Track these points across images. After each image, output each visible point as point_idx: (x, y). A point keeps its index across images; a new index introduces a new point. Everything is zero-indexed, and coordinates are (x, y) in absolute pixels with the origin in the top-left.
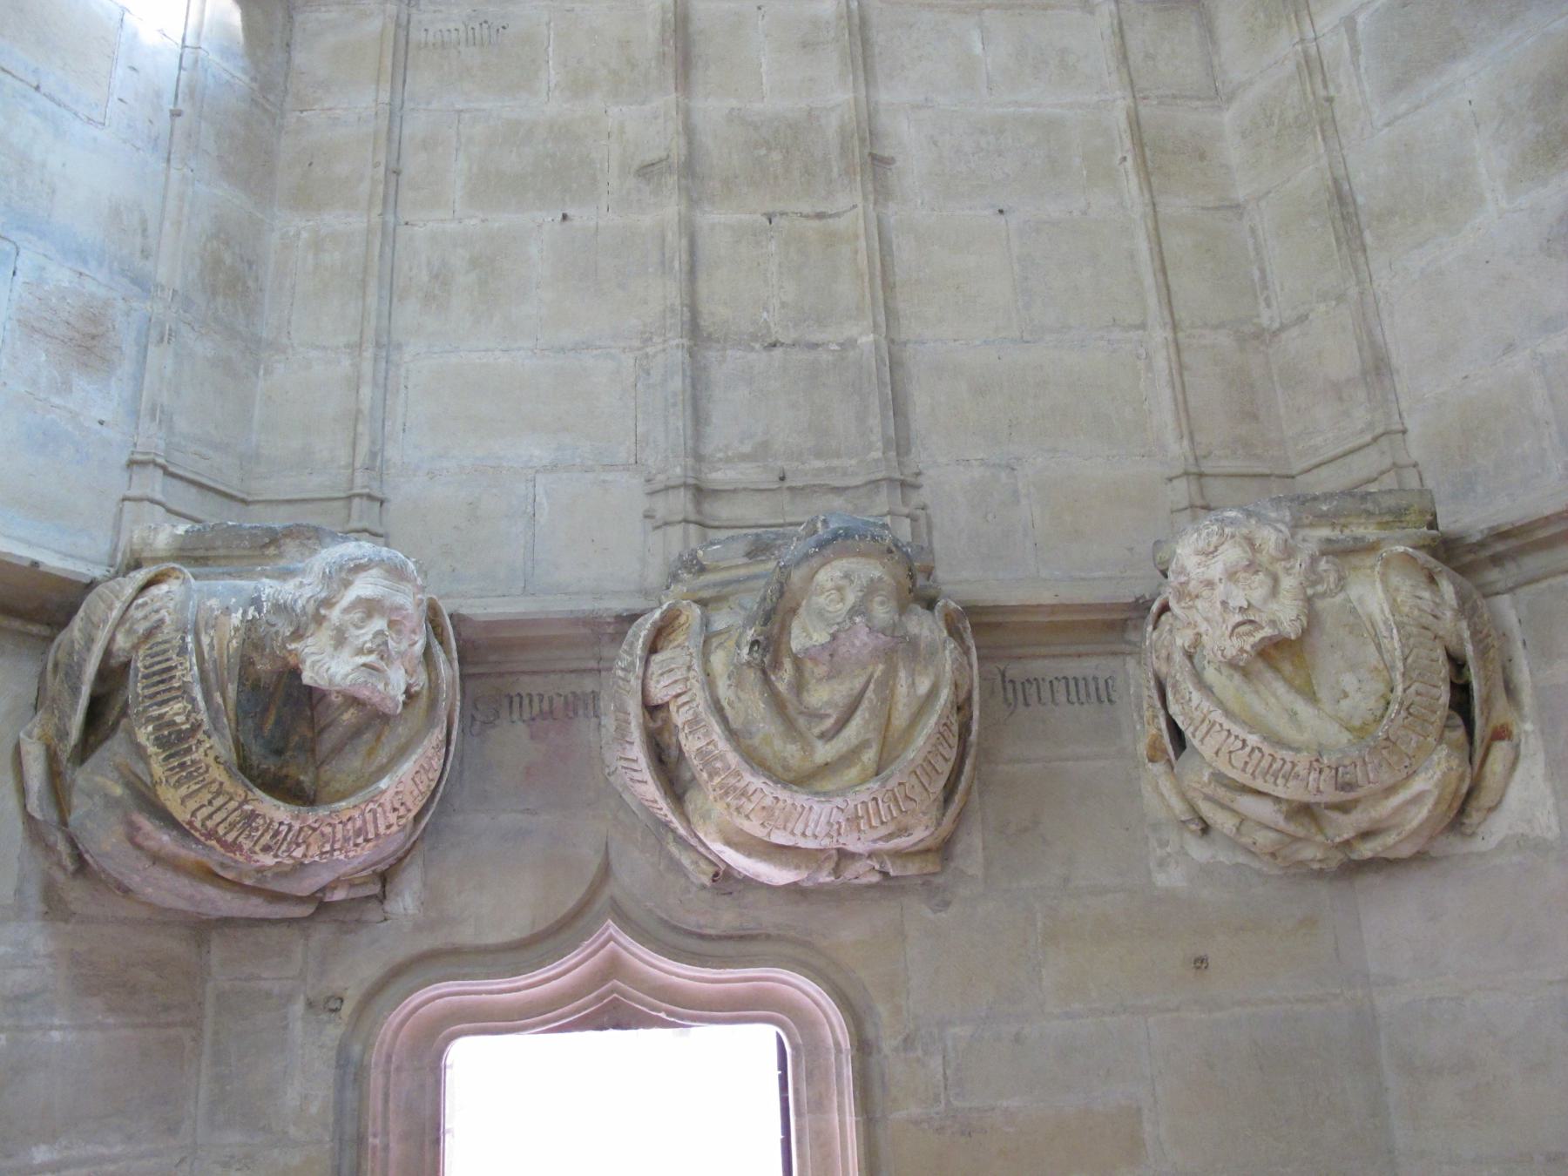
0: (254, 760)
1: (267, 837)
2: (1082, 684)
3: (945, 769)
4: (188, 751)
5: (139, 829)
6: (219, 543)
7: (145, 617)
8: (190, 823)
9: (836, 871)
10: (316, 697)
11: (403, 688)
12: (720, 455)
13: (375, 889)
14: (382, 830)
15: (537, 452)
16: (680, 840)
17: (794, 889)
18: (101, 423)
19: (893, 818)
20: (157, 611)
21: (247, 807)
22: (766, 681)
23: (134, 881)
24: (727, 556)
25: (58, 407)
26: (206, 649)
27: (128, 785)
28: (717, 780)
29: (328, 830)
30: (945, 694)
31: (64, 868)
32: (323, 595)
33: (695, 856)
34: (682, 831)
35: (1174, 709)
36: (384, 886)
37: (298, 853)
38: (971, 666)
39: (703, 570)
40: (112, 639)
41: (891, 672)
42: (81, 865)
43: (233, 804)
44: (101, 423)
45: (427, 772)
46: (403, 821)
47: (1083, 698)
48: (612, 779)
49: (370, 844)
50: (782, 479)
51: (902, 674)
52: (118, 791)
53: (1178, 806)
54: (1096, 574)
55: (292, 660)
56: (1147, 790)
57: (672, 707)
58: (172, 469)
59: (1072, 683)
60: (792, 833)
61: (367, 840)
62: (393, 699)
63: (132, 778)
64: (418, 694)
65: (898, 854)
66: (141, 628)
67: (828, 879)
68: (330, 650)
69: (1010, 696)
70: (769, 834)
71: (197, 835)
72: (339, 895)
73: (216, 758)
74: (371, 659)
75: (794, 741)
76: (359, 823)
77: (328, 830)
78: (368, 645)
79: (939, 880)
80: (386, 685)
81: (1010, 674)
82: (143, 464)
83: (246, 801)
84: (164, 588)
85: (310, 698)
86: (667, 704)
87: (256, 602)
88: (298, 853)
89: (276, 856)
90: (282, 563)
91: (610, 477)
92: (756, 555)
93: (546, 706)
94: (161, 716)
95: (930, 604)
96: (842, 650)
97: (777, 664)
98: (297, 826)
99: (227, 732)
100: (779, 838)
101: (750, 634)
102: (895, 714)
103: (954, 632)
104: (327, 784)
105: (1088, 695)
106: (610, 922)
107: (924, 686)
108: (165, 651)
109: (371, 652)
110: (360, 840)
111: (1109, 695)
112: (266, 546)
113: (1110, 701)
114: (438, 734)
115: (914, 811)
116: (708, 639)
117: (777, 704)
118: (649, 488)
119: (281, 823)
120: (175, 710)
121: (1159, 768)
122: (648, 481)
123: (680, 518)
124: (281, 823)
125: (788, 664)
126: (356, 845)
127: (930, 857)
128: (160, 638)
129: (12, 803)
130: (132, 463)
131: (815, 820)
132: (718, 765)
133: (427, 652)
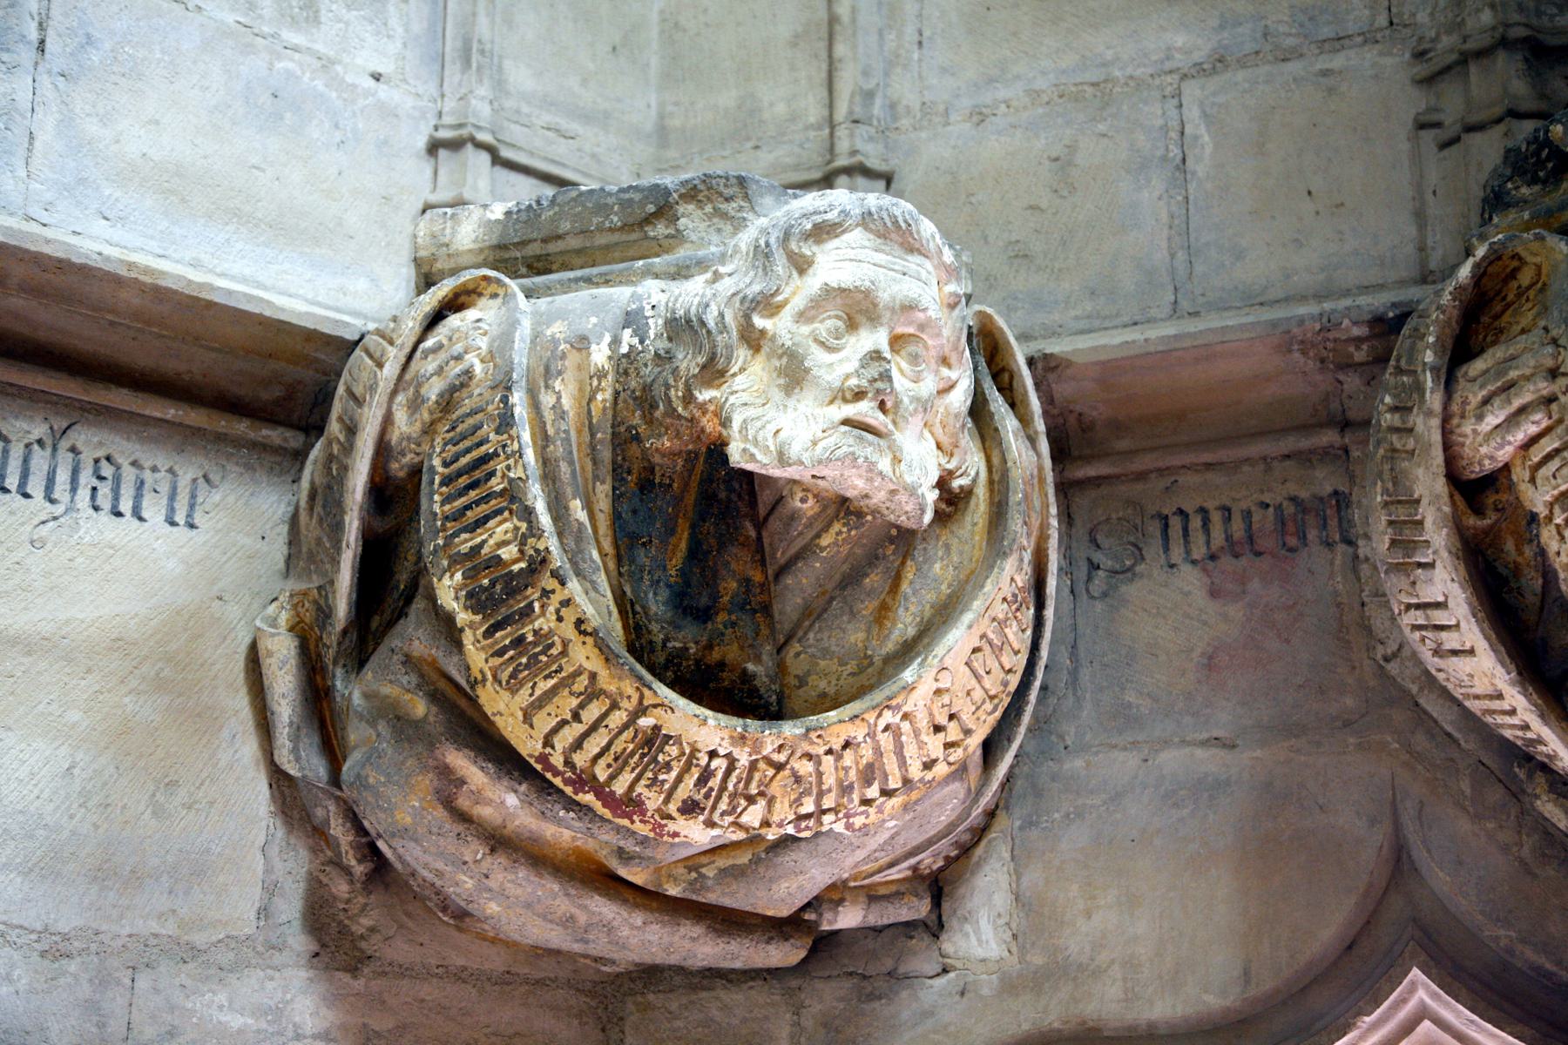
0: (657, 632)
1: (690, 781)
4: (527, 612)
5: (462, 782)
6: (566, 226)
7: (440, 371)
8: (543, 759)
10: (765, 498)
11: (934, 476)
13: (919, 908)
14: (915, 771)
15: (1180, 40)
18: (377, 77)
20: (458, 358)
21: (645, 722)
23: (462, 886)
25: (296, 49)
26: (549, 416)
27: (435, 697)
29: (805, 768)
31: (347, 871)
32: (756, 288)
36: (937, 901)
37: (753, 816)
40: (388, 420)
42: (380, 870)
43: (618, 718)
44: (377, 77)
45: (997, 651)
46: (957, 755)
48: (1393, 668)
49: (896, 801)
52: (420, 707)
55: (709, 425)
57: (1520, 474)
58: (506, 153)
61: (887, 793)
62: (912, 491)
63: (442, 684)
64: (967, 493)
66: (433, 390)
68: (777, 395)
71: (558, 781)
72: (849, 918)
73: (579, 622)
74: (864, 409)
76: (867, 753)
77: (805, 768)
78: (853, 382)
80: (897, 460)
82: (455, 145)
83: (641, 710)
84: (471, 314)
85: (753, 503)
86: (1507, 467)
87: (632, 319)
88: (753, 816)
89: (710, 824)
90: (682, 253)
91: (1338, 62)
93: (1238, 528)
94: (476, 550)
98: (744, 759)
99: (602, 579)
104: (802, 682)
106: (1416, 973)
108: (479, 427)
109: (859, 395)
110: (873, 792)
112: (648, 220)
114: (1012, 574)
118: (1422, 70)
119: (713, 754)
120: (500, 537)
122: (1420, 55)
123: (1498, 111)
124: (713, 754)
126: (867, 802)
128: (468, 405)
129: (249, 748)
130: (434, 147)
133: (978, 411)
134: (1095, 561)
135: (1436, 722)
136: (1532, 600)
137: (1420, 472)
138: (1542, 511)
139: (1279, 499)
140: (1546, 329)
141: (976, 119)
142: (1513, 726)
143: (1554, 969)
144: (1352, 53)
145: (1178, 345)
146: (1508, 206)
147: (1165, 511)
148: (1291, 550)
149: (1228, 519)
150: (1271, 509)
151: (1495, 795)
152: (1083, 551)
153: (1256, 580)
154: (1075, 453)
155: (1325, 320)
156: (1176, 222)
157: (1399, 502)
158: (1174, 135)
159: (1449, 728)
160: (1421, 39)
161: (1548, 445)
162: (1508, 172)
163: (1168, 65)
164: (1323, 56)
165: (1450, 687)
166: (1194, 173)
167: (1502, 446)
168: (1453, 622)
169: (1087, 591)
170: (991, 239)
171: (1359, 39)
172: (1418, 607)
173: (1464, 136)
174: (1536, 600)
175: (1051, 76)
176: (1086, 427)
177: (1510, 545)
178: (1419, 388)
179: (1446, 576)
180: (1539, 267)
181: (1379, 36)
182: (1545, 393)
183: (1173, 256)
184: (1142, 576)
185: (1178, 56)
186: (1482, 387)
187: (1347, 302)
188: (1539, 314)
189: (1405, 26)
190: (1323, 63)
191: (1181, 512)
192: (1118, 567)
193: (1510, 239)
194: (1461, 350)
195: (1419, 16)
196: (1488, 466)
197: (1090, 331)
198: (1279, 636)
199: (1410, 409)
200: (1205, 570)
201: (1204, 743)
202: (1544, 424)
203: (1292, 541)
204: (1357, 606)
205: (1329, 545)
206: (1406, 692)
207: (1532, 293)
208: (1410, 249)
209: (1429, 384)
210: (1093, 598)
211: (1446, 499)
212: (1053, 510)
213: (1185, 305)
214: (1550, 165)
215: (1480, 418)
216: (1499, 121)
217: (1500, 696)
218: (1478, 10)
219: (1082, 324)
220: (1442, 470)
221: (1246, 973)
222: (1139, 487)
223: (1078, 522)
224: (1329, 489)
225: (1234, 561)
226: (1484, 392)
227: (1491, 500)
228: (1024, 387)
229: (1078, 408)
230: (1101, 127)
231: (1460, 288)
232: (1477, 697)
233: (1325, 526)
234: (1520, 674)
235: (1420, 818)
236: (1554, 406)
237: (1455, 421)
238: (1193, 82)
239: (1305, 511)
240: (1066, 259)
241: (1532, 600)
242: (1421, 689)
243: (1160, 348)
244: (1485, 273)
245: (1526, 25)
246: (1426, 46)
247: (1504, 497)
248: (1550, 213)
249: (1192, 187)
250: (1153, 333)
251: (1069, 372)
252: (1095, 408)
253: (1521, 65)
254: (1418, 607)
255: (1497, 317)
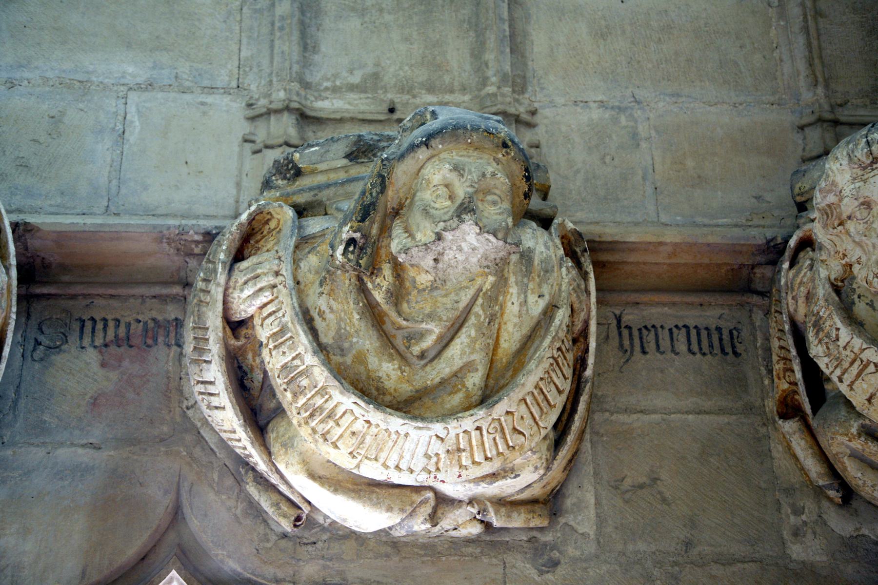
2: (704, 334)
3: (559, 402)
9: (433, 518)
12: (326, 84)
15: (130, 69)
16: (262, 481)
17: (384, 539)
19: (499, 454)
22: (362, 290)
24: (325, 160)
28: (302, 401)
30: (561, 316)
33: (275, 497)
34: (262, 467)
35: (816, 350)
38: (588, 293)
39: (298, 173)
41: (502, 282)
47: (706, 349)
48: (190, 413)
50: (392, 110)
51: (514, 290)
53: (813, 467)
54: (721, 221)
56: (777, 450)
57: (257, 321)
59: (693, 332)
60: (386, 466)
65: (503, 503)
67: (423, 527)
69: (626, 343)
70: (358, 466)
75: (391, 359)
79: (548, 537)
81: (627, 319)
86: (252, 317)
91: (210, 99)
92: (356, 158)
93: (122, 332)
95: (545, 222)
96: (449, 255)
97: (374, 270)
100: (371, 471)
101: (346, 233)
102: (504, 336)
103: (571, 253)
105: (711, 346)
106: (174, 573)
107: (537, 306)
111: (733, 347)
113: (736, 354)
115: (522, 447)
116: (304, 243)
117: (374, 316)
118: (250, 113)
121: (790, 426)
122: (250, 105)
123: (281, 141)
125: (387, 270)
127: (537, 507)
131: (408, 449)
132: (305, 382)
134: (39, 340)
135: (207, 442)
136: (257, 384)
137: (210, 314)
138: (265, 341)
139: (147, 319)
140: (277, 251)
141: (8, 85)
142: (240, 447)
143: (241, 571)
144: (217, 96)
145: (102, 229)
146: (271, 188)
147: (84, 318)
148: (148, 346)
149: (117, 326)
150: (141, 324)
151: (229, 481)
152: (33, 334)
153: (128, 360)
154: (37, 279)
155: (181, 229)
156: (115, 164)
157: (200, 328)
158: (120, 118)
159: (213, 446)
160: (251, 97)
161: (270, 308)
162: (274, 171)
163: (123, 81)
164: (203, 95)
165: (214, 425)
166: (128, 140)
167: (250, 306)
168: (217, 392)
169: (32, 356)
170: (7, 153)
171: (222, 91)
172: (203, 383)
173: (264, 150)
174: (259, 385)
175: (57, 72)
176: (46, 266)
177: (250, 356)
178: (215, 271)
179: (216, 369)
180: (279, 220)
181: (232, 91)
182: (272, 282)
183: (110, 182)
184: (65, 351)
185: (128, 77)
186: (245, 275)
187: (194, 222)
188: (276, 244)
189: (245, 90)
190: (203, 98)
191: (93, 319)
192: (52, 345)
193: (268, 204)
194: (239, 256)
195: (252, 86)
196: (244, 316)
197: (57, 214)
198: (134, 391)
199: (210, 281)
200: (100, 352)
201: (83, 446)
202: (270, 298)
203: (150, 342)
204: (177, 379)
205: (169, 346)
206: (194, 426)
207: (274, 233)
208: (231, 201)
209: (220, 270)
210: (34, 360)
211: (221, 329)
212: (14, 309)
213: (113, 208)
214: (292, 172)
215: (242, 290)
216: (281, 146)
217: (234, 432)
218: (279, 90)
219: (53, 210)
220: (221, 314)
221: (84, 573)
222: (71, 302)
223: (33, 318)
224: (173, 317)
225: (117, 349)
226: (245, 278)
227: (243, 333)
228: (7, 238)
229: (43, 255)
230: (81, 106)
231: (241, 224)
232: (225, 431)
233: (168, 335)
234: (245, 421)
235: (190, 491)
236: (275, 290)
237: (231, 291)
238: (134, 93)
239: (159, 327)
240: (50, 172)
241: (257, 384)
242: (202, 425)
243: (92, 229)
244: (254, 219)
245: (299, 103)
246: (253, 102)
247: (250, 332)
248: (288, 195)
249: (126, 147)
250: (89, 220)
251: (38, 234)
252: (52, 256)
253: (294, 121)
254: (203, 383)
255: (257, 242)
